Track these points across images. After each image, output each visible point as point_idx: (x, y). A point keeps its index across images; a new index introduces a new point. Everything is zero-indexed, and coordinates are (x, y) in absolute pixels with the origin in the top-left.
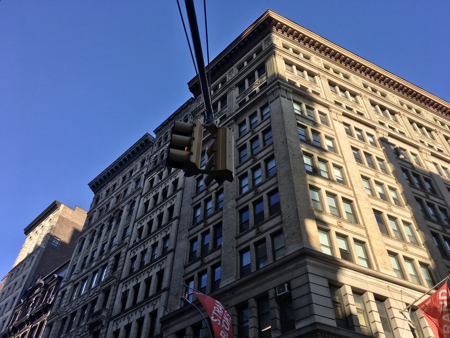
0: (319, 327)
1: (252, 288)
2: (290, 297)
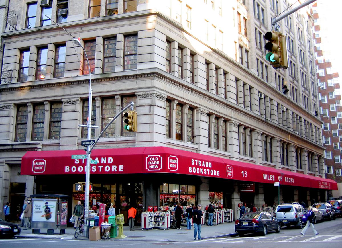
0: (157, 71)
1: (101, 29)
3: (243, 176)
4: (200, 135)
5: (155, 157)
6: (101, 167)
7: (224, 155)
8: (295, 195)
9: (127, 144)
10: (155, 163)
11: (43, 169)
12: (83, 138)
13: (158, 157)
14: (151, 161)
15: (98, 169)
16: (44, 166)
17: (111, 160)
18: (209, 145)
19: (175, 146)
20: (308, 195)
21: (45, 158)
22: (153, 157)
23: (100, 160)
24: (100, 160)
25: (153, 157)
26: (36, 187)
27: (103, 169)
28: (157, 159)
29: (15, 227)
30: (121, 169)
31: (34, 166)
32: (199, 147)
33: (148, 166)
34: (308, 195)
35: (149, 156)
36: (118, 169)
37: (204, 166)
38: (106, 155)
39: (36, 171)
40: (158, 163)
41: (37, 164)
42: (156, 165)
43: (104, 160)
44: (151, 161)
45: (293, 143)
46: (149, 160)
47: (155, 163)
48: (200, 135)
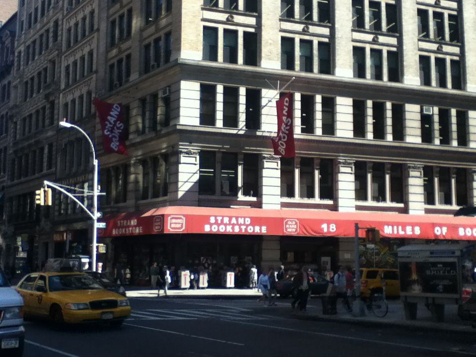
2: (169, 98)
3: (180, 143)
5: (292, 221)
6: (243, 227)
8: (264, 249)
10: (293, 226)
11: (182, 227)
12: (34, 111)
13: (295, 221)
14: (289, 225)
15: (241, 230)
16: (182, 224)
17: (248, 221)
20: (369, 124)
21: (184, 215)
22: (290, 221)
23: (237, 221)
24: (237, 221)
25: (290, 221)
27: (246, 229)
28: (294, 223)
29: (18, 272)
30: (39, 195)
31: (171, 224)
33: (286, 229)
34: (369, 124)
35: (287, 220)
36: (261, 230)
38: (244, 216)
39: (172, 228)
40: (295, 226)
41: (174, 221)
42: (293, 228)
43: (241, 221)
44: (289, 225)
45: (222, 316)
46: (286, 224)
47: (293, 226)
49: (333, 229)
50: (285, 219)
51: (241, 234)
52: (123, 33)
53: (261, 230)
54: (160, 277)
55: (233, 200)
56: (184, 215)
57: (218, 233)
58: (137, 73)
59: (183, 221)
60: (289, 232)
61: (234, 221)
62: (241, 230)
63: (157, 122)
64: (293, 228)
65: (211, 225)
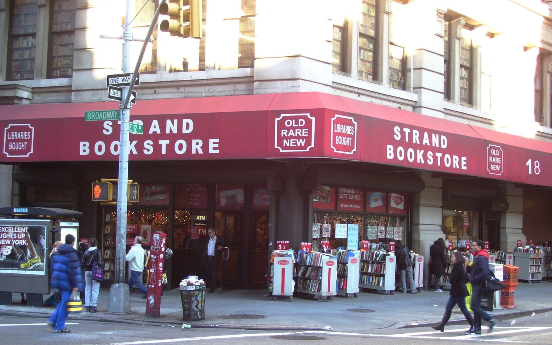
4: (422, 68)
5: (297, 119)
7: (484, 120)
9: (233, 86)
10: (298, 132)
13: (305, 118)
15: (157, 147)
16: (29, 141)
18: (448, 94)
19: (356, 93)
21: (33, 122)
22: (291, 118)
23: (163, 126)
24: (163, 126)
25: (291, 118)
26: (17, 191)
27: (170, 148)
28: (302, 122)
31: (8, 142)
32: (420, 97)
36: (205, 147)
37: (429, 144)
39: (11, 152)
41: (14, 135)
42: (298, 137)
46: (281, 125)
47: (298, 132)
48: (422, 68)
49: (85, 151)
50: (277, 113)
51: (159, 159)
52: (443, 336)
53: (205, 147)
54: (22, 250)
55: (19, 15)
56: (33, 122)
57: (107, 160)
58: (449, 321)
59: (30, 135)
60: (492, 171)
61: (155, 127)
62: (157, 147)
63: (485, 310)
64: (298, 137)
65: (396, 144)
